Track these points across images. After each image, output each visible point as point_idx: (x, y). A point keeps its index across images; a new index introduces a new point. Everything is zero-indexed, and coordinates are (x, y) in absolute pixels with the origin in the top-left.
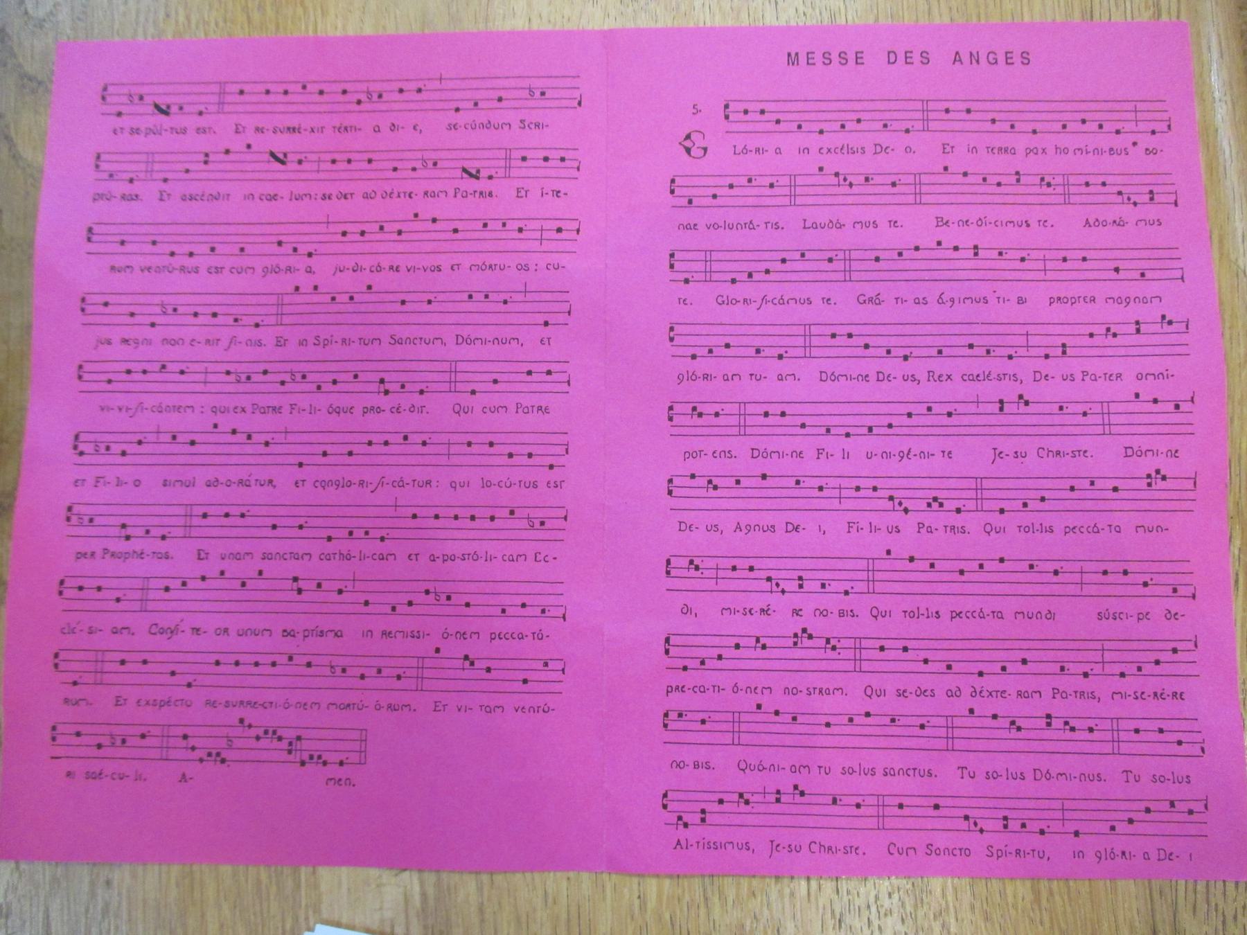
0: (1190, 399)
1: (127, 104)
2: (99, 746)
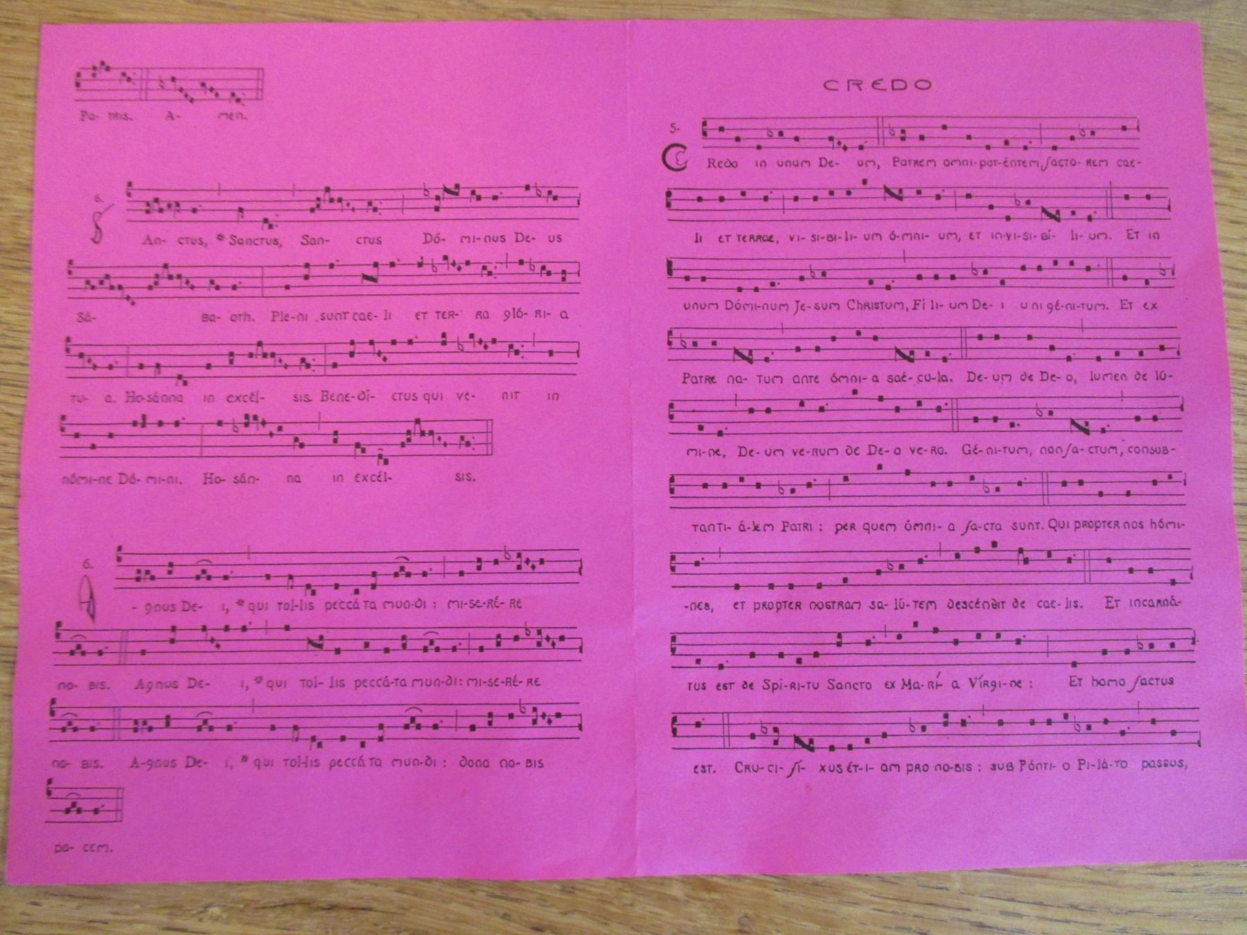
0: (577, 570)
1: (158, 90)
2: (511, 716)
